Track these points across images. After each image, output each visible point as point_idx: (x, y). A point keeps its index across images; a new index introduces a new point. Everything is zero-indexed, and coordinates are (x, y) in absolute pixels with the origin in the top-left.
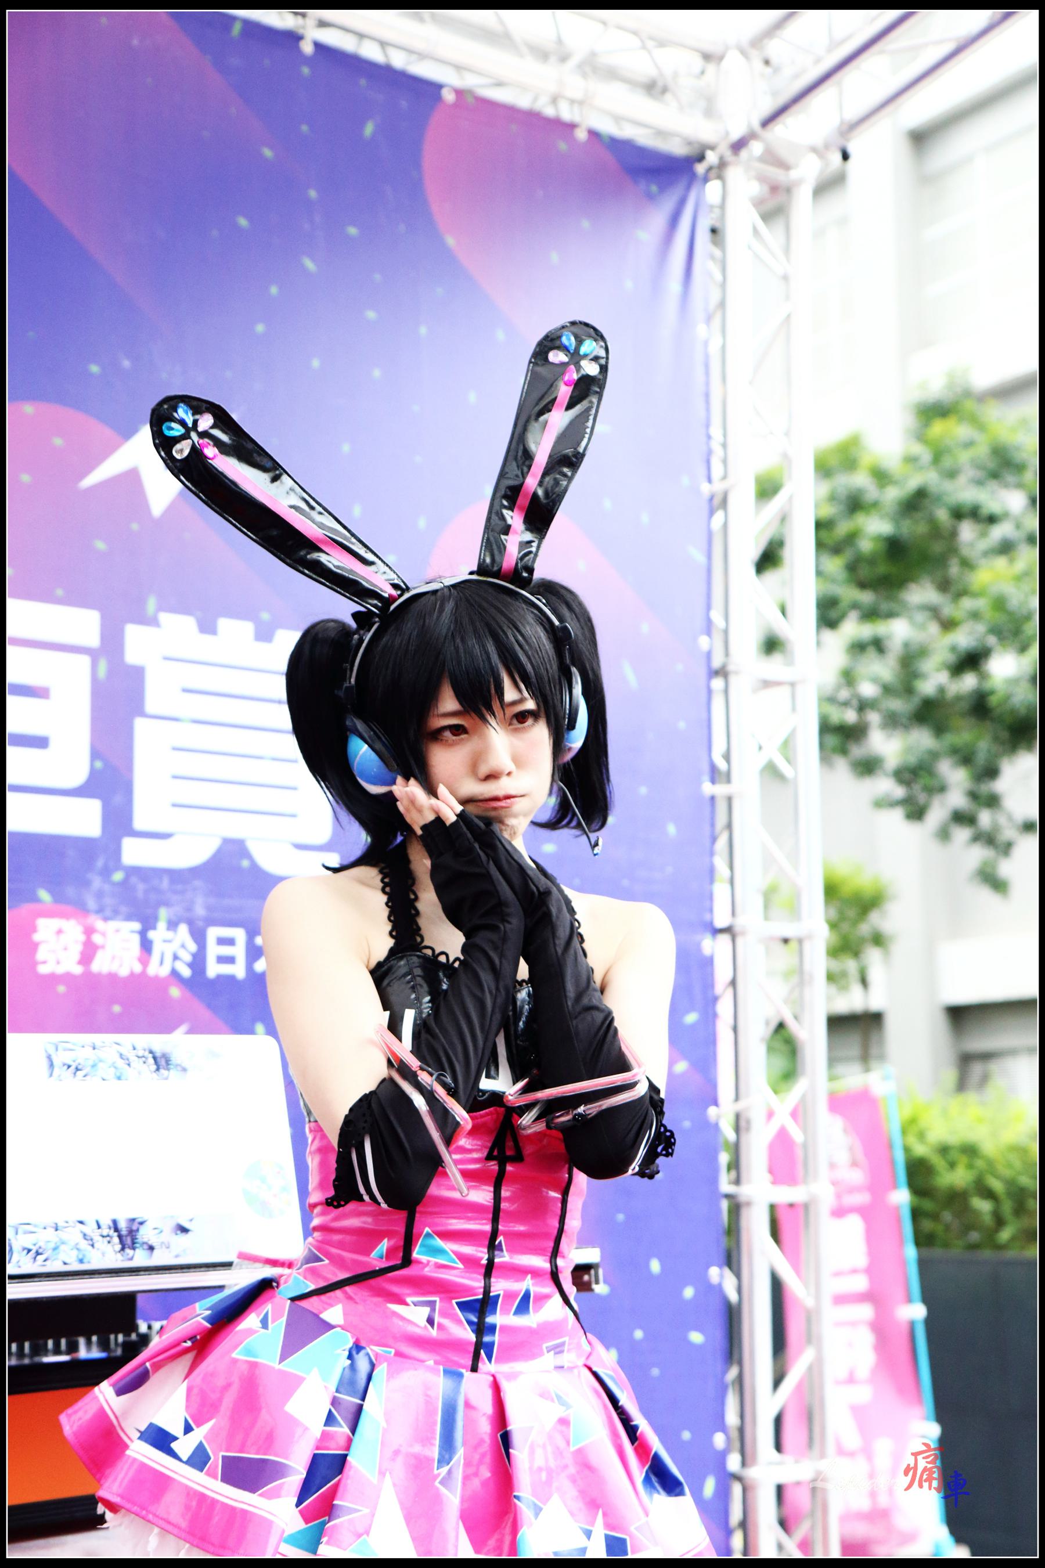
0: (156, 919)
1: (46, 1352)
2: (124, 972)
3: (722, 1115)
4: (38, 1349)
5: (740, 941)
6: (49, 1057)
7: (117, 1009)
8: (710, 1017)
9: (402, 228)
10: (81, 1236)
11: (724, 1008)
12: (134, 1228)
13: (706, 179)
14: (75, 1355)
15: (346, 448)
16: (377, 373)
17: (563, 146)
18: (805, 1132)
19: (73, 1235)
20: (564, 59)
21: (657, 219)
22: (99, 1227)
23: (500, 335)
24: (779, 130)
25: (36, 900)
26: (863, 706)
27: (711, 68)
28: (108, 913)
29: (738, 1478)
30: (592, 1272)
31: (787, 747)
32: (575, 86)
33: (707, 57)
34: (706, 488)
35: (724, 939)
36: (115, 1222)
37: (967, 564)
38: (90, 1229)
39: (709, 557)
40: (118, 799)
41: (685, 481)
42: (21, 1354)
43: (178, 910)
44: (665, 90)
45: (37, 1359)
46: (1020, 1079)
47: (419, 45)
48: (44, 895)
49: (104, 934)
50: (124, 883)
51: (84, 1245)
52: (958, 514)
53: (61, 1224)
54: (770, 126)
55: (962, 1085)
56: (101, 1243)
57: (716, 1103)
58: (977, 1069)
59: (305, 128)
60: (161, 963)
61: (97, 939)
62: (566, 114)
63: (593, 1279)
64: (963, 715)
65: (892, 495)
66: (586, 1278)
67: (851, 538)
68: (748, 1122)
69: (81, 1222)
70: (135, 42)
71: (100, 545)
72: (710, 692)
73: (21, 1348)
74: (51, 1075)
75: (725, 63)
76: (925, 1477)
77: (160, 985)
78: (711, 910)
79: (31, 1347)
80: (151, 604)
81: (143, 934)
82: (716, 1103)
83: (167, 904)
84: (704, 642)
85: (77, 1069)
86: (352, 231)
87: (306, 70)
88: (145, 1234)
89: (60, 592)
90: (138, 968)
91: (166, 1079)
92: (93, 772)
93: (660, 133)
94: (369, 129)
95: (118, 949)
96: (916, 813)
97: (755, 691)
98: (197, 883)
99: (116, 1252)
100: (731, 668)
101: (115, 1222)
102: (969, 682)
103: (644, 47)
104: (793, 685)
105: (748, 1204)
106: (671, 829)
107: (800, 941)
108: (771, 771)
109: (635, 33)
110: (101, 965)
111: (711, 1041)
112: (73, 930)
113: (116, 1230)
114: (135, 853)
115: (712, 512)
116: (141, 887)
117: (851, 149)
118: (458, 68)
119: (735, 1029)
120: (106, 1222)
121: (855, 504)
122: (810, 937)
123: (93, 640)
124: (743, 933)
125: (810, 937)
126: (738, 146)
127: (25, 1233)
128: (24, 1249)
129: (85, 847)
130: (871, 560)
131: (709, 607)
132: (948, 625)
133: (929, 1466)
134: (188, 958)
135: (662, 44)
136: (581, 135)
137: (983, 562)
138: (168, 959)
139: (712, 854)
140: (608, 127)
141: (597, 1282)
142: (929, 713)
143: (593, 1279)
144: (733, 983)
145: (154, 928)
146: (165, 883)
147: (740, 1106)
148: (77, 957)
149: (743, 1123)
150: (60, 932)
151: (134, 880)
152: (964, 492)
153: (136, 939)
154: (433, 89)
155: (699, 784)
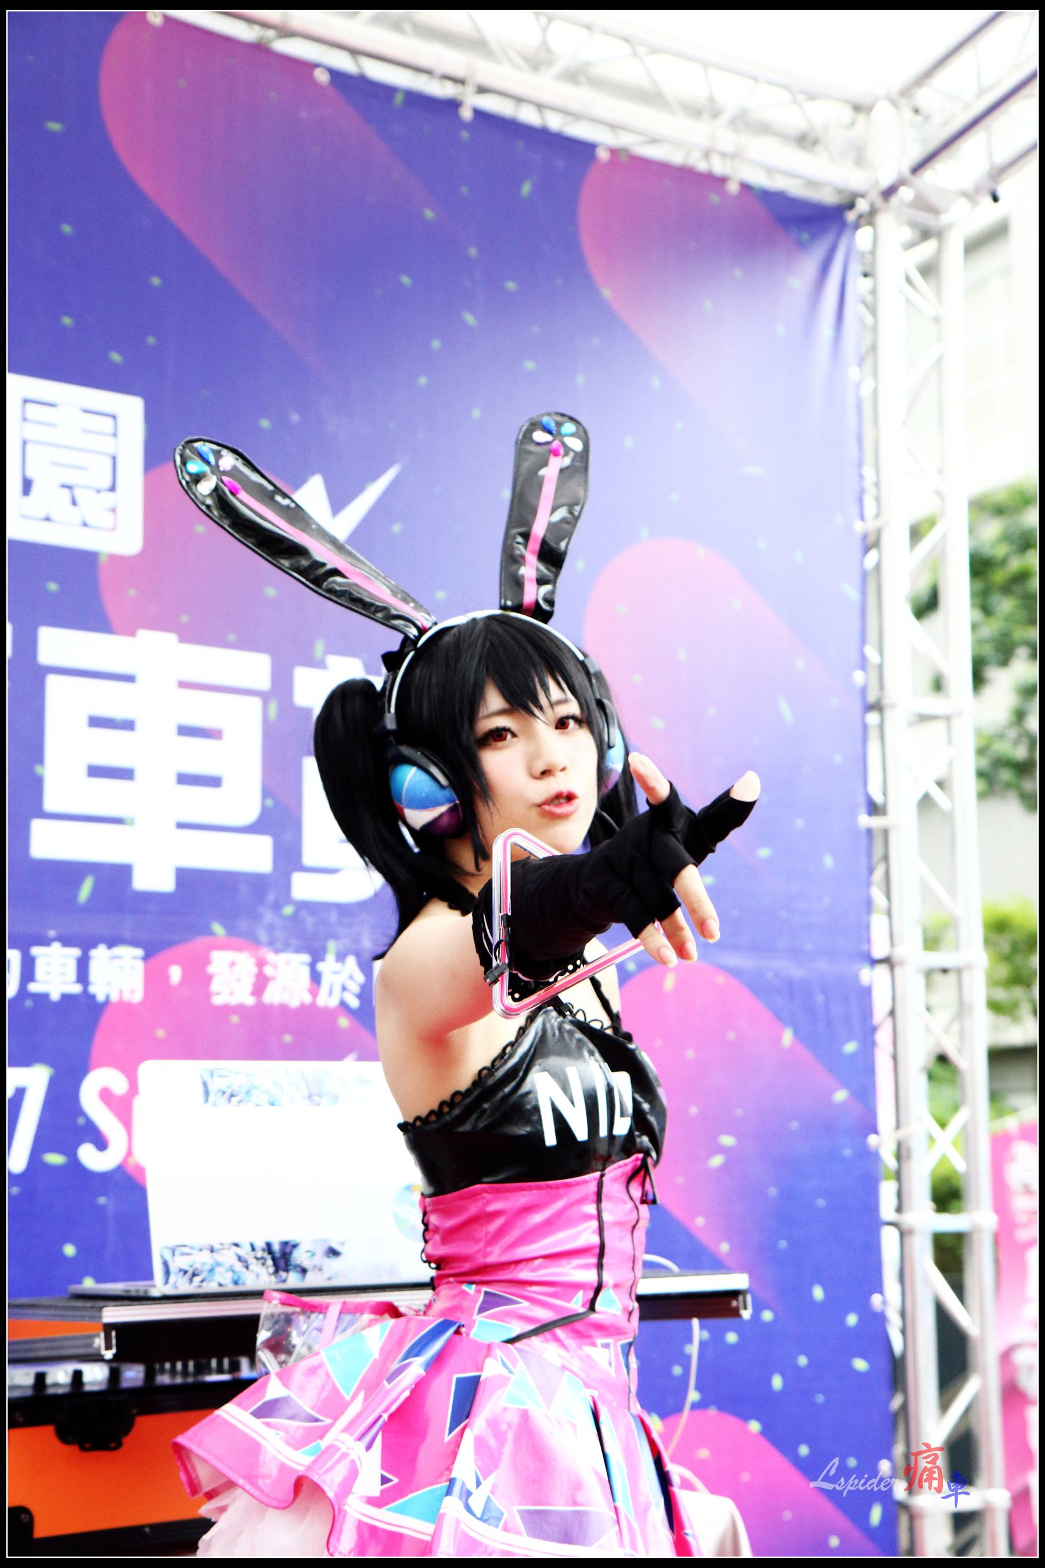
0: (324, 950)
1: (209, 1371)
2: (294, 1003)
3: (883, 1143)
4: (203, 1368)
5: (898, 971)
6: (205, 1084)
7: (288, 1038)
8: (869, 1045)
9: (559, 282)
10: (236, 1258)
11: (883, 1038)
12: (288, 1250)
13: (856, 226)
14: (236, 1375)
17: (715, 199)
19: (228, 1258)
20: (716, 114)
21: (808, 265)
22: (253, 1249)
23: (656, 382)
24: (930, 176)
25: (209, 932)
27: (861, 119)
28: (279, 945)
29: (904, 1506)
30: (741, 1298)
32: (726, 140)
33: (857, 108)
34: (859, 527)
35: (882, 970)
38: (245, 1251)
40: (288, 836)
41: (839, 519)
42: (185, 1373)
43: (346, 942)
44: (815, 142)
45: (200, 1378)
47: (574, 106)
48: (218, 929)
49: (275, 966)
50: (295, 917)
51: (238, 1266)
53: (216, 1246)
54: (920, 172)
56: (255, 1266)
57: (875, 1131)
59: (464, 190)
60: (330, 994)
61: (268, 971)
62: (718, 167)
63: (741, 1305)
66: (734, 1303)
68: (909, 1150)
69: (236, 1245)
70: (303, 114)
72: (865, 727)
73: (185, 1366)
74: (206, 1101)
75: (875, 113)
76: (925, 1477)
77: (329, 1015)
78: (869, 940)
79: (196, 1366)
80: (319, 648)
81: (313, 966)
82: (875, 1131)
83: (336, 937)
84: (859, 677)
86: (511, 286)
87: (465, 135)
88: (299, 1257)
90: (308, 999)
91: (318, 1105)
92: (264, 810)
93: (812, 183)
94: (526, 189)
95: (289, 980)
97: (911, 725)
98: (364, 916)
99: (270, 1275)
100: (886, 701)
103: (794, 101)
104: (948, 718)
106: (829, 861)
108: (926, 802)
109: (786, 88)
110: (272, 996)
114: (304, 887)
115: (866, 550)
116: (310, 921)
117: (1000, 193)
118: (614, 127)
119: (895, 1058)
120: (260, 1244)
122: (970, 967)
123: (264, 683)
125: (970, 967)
126: (888, 193)
127: (183, 1254)
128: (181, 1270)
129: (257, 883)
133: (929, 1466)
134: (356, 989)
135: (812, 97)
136: (733, 188)
138: (337, 990)
139: (869, 885)
140: (759, 179)
141: (745, 1308)
143: (741, 1305)
144: (892, 1013)
145: (323, 960)
146: (333, 917)
147: (902, 1133)
149: (904, 1152)
150: (233, 964)
151: (303, 913)
153: (306, 971)
154: (584, 150)
155: (855, 817)
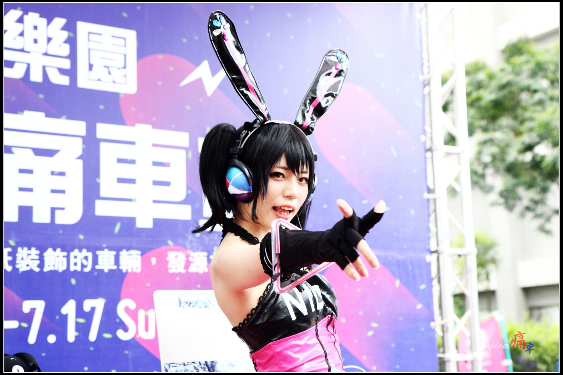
2: (201, 272)
15: (281, 67)
16: (292, 37)
18: (471, 332)
22: (200, 364)
23: (339, 21)
25: (167, 244)
26: (486, 166)
28: (195, 249)
31: (457, 180)
34: (421, 78)
35: (435, 256)
36: (206, 362)
37: (525, 109)
39: (424, 103)
40: (197, 205)
46: (553, 316)
48: (170, 243)
52: (522, 90)
53: (186, 363)
55: (531, 316)
57: (433, 320)
58: (536, 313)
61: (191, 259)
64: (526, 169)
65: (494, 84)
67: (479, 99)
68: (447, 328)
69: (193, 363)
71: (188, 108)
72: (426, 158)
78: (429, 244)
81: (208, 257)
82: (433, 320)
84: (423, 138)
85: (190, 304)
89: (173, 126)
96: (510, 208)
100: (434, 148)
101: (206, 362)
102: (528, 157)
104: (458, 154)
105: (449, 361)
106: (412, 212)
107: (465, 256)
111: (431, 296)
112: (181, 256)
113: (207, 365)
115: (424, 87)
120: (203, 362)
121: (479, 86)
123: (186, 144)
124: (443, 253)
127: (173, 366)
130: (486, 109)
131: (424, 124)
132: (518, 134)
137: (533, 108)
139: (429, 222)
142: (512, 169)
147: (444, 322)
148: (183, 266)
149: (445, 329)
150: (176, 257)
152: (524, 80)
153: (206, 259)
155: (422, 194)
